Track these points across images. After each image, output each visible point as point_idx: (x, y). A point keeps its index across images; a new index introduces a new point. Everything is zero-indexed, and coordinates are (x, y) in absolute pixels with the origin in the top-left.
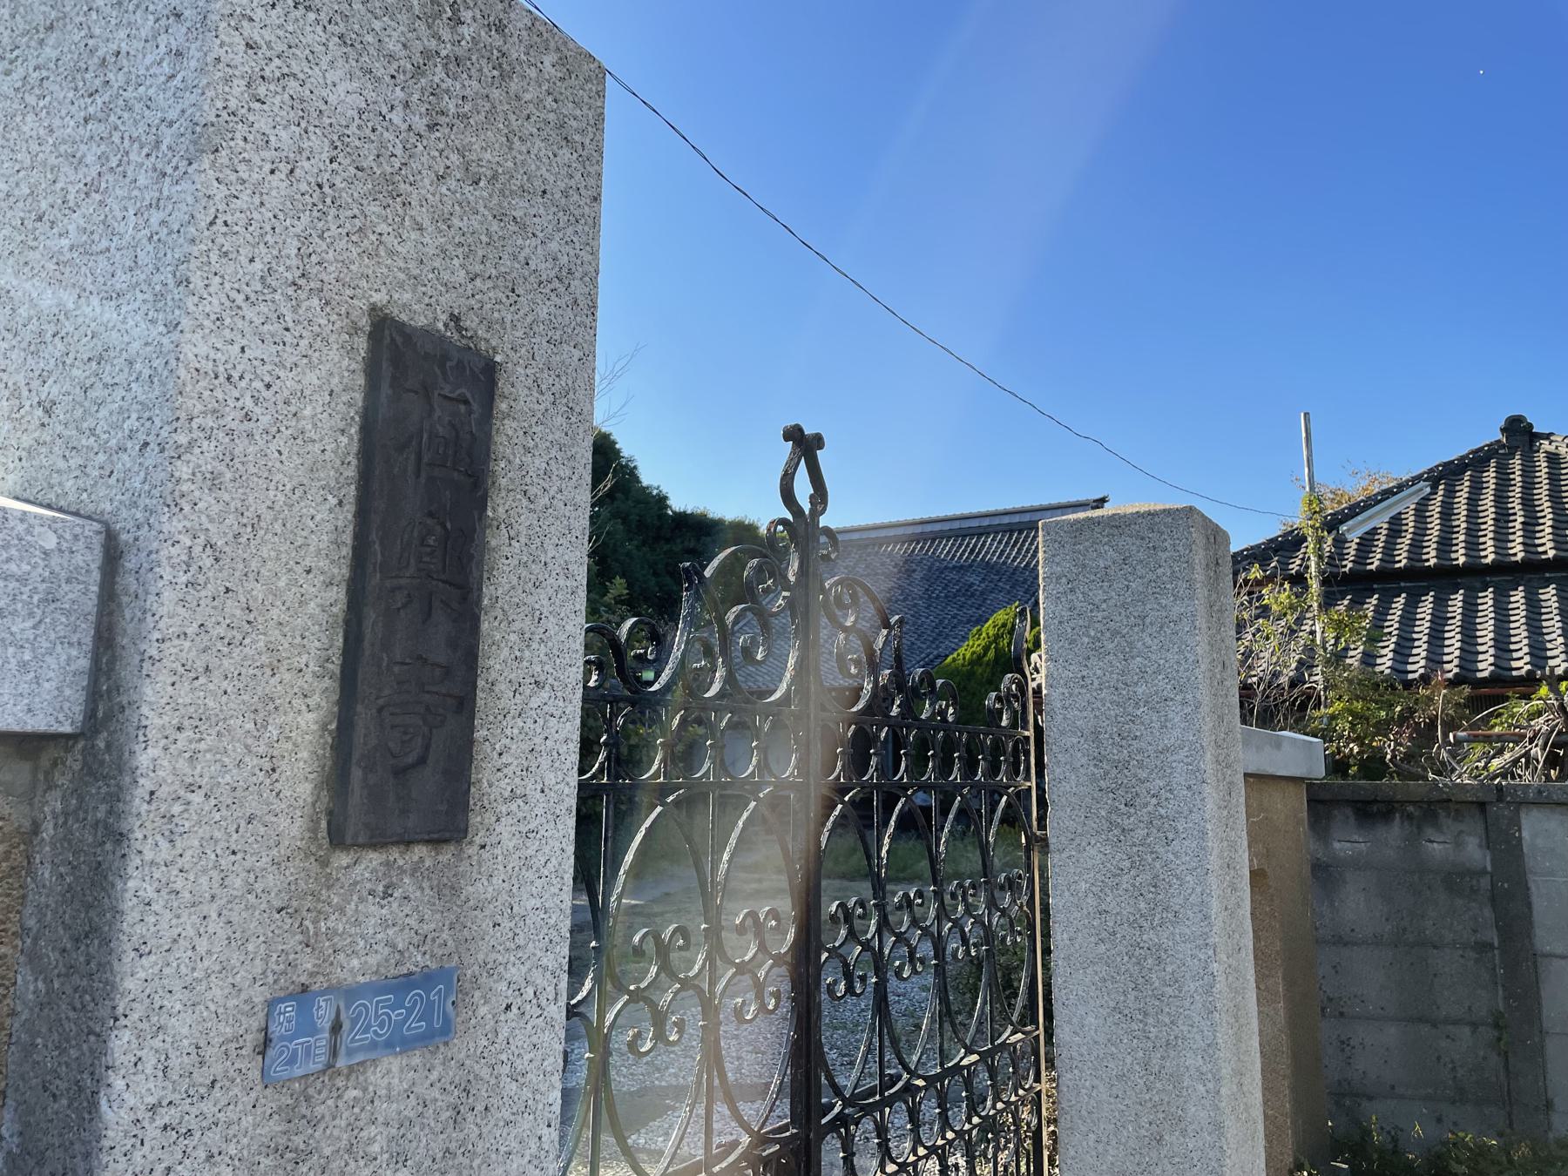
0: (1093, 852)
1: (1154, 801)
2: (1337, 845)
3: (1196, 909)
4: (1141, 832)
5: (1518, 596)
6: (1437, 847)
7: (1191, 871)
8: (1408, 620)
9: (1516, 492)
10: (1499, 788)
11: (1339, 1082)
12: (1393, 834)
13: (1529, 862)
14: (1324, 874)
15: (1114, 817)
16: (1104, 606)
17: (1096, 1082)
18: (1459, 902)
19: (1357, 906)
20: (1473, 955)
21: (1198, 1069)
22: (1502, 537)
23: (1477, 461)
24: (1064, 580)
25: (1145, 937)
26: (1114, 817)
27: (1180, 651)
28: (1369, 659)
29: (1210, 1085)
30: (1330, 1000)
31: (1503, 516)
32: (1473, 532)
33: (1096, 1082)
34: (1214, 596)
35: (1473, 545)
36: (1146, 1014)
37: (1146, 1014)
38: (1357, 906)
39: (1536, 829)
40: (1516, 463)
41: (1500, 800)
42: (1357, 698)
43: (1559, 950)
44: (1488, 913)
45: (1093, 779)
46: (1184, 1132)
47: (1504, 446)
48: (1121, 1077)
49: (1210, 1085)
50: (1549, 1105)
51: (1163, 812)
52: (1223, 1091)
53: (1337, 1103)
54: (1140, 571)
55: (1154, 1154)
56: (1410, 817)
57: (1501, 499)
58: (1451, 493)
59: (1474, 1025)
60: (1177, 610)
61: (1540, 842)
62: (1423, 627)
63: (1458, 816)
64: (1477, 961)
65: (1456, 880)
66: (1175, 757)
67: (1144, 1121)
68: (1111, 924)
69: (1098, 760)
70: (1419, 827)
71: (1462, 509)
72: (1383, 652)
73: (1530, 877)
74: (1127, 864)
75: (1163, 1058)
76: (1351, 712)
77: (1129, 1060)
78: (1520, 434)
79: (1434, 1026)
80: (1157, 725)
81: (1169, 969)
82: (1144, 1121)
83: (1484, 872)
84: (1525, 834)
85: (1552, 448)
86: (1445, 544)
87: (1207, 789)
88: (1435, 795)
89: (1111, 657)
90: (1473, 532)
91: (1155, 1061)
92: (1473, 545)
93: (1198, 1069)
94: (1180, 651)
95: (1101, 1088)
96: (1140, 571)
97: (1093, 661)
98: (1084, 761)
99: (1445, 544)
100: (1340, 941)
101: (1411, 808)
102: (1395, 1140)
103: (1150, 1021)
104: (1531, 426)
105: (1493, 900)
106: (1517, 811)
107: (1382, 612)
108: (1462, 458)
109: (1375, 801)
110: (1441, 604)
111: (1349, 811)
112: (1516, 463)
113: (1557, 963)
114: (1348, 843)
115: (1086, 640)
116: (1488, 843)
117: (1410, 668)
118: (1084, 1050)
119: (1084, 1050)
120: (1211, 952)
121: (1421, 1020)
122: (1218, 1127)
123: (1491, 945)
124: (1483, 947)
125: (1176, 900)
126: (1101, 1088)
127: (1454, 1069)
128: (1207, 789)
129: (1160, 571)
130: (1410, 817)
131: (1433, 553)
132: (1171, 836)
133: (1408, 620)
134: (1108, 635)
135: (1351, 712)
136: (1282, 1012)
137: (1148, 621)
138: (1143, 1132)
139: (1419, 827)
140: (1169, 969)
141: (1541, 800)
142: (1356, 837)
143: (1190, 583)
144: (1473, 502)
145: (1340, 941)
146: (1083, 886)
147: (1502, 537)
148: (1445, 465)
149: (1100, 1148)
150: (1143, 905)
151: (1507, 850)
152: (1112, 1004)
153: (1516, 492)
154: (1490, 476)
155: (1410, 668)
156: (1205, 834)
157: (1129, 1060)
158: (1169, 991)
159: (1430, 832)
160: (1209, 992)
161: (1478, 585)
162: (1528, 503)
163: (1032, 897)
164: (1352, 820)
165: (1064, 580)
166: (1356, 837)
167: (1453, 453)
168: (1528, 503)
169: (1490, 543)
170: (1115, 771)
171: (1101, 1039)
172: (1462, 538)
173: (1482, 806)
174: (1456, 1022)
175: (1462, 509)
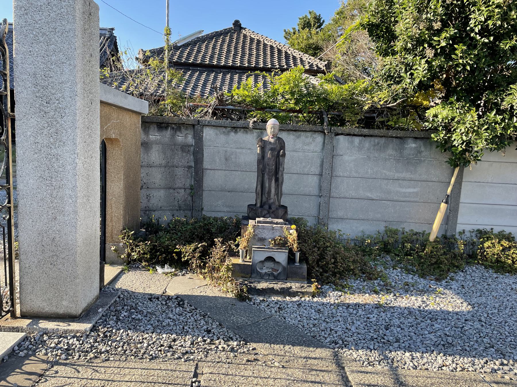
0: (32, 120)
1: (57, 102)
2: (151, 136)
3: (71, 141)
4: (52, 113)
5: (228, 76)
6: (180, 138)
7: (70, 128)
8: (198, 79)
9: (233, 44)
10: (198, 121)
11: (146, 207)
12: (168, 133)
13: (204, 143)
14: (146, 145)
15: (41, 107)
16: (40, 22)
17: (33, 202)
18: (184, 154)
19: (155, 156)
20: (187, 169)
21: (69, 195)
22: (227, 58)
23: (225, 33)
24: (23, 9)
25: (52, 151)
26: (41, 107)
27: (69, 44)
28: (184, 89)
29: (74, 199)
30: (145, 183)
31: (229, 51)
32: (220, 55)
33: (33, 202)
34: (87, 27)
35: (219, 59)
36: (52, 178)
37: (52, 178)
38: (155, 156)
39: (208, 134)
40: (235, 36)
41: (198, 124)
42: (175, 99)
43: (209, 167)
44: (192, 157)
45: (34, 92)
46: (64, 215)
47: (233, 30)
48: (42, 200)
49: (74, 199)
50: (202, 209)
51: (60, 106)
52: (78, 201)
53: (144, 213)
54: (55, 9)
55: (53, 223)
56: (173, 128)
57: (229, 46)
58: (216, 42)
59: (185, 189)
60: (68, 27)
61: (208, 137)
62: (201, 82)
63: (187, 129)
64: (187, 171)
65: (184, 148)
66: (66, 86)
67: (50, 213)
68: (39, 147)
69: (36, 85)
70: (175, 132)
71: (218, 47)
72: (189, 88)
73: (204, 147)
74: (46, 125)
75: (57, 192)
76: (172, 103)
77: (45, 193)
78: (238, 26)
79: (174, 189)
80: (59, 73)
81: (61, 162)
82: (50, 213)
83: (192, 145)
84: (204, 135)
85: (245, 33)
86: (212, 57)
87: (77, 98)
88: (180, 122)
89: (42, 44)
90: (220, 55)
91: (55, 193)
92: (219, 59)
93: (69, 195)
94: (69, 44)
95: (35, 204)
96: (55, 9)
97: (35, 45)
98: (30, 85)
99: (212, 57)
100: (150, 166)
101: (174, 126)
102: (158, 221)
103: (53, 180)
104: (241, 24)
105: (194, 154)
106: (203, 128)
107: (191, 76)
108: (221, 31)
109: (163, 123)
110: (208, 75)
111: (155, 126)
112: (235, 36)
113: (208, 171)
114: (154, 136)
115: (32, 36)
116: (194, 137)
117: (195, 94)
118: (28, 191)
119: (28, 191)
120: (76, 156)
121: (170, 188)
122: (76, 212)
123: (192, 167)
124: (190, 167)
125: (64, 138)
126: (35, 204)
127: (178, 201)
128: (77, 98)
129: (62, 10)
130: (173, 128)
131: (208, 60)
132: (63, 115)
133: (198, 79)
134: (41, 34)
135: (172, 103)
136: (122, 185)
137: (57, 30)
138: (50, 217)
139: (175, 132)
140: (61, 162)
141: (209, 125)
142: (156, 134)
143: (74, 17)
144: (222, 45)
145: (150, 166)
146: (29, 133)
147: (227, 58)
148: (216, 32)
149: (34, 223)
150: (52, 140)
151: (199, 139)
152: (39, 175)
153: (233, 44)
154: (228, 38)
155: (195, 94)
156: (76, 114)
157: (45, 193)
158: (61, 169)
159: (178, 133)
160: (74, 169)
161: (219, 72)
162: (236, 48)
163: (7, 137)
164: (156, 128)
165: (23, 9)
166: (156, 134)
167: (219, 29)
168: (236, 48)
169: (224, 59)
170: (42, 90)
171: (35, 187)
172: (217, 56)
173: (194, 126)
174: (180, 188)
175: (218, 47)
